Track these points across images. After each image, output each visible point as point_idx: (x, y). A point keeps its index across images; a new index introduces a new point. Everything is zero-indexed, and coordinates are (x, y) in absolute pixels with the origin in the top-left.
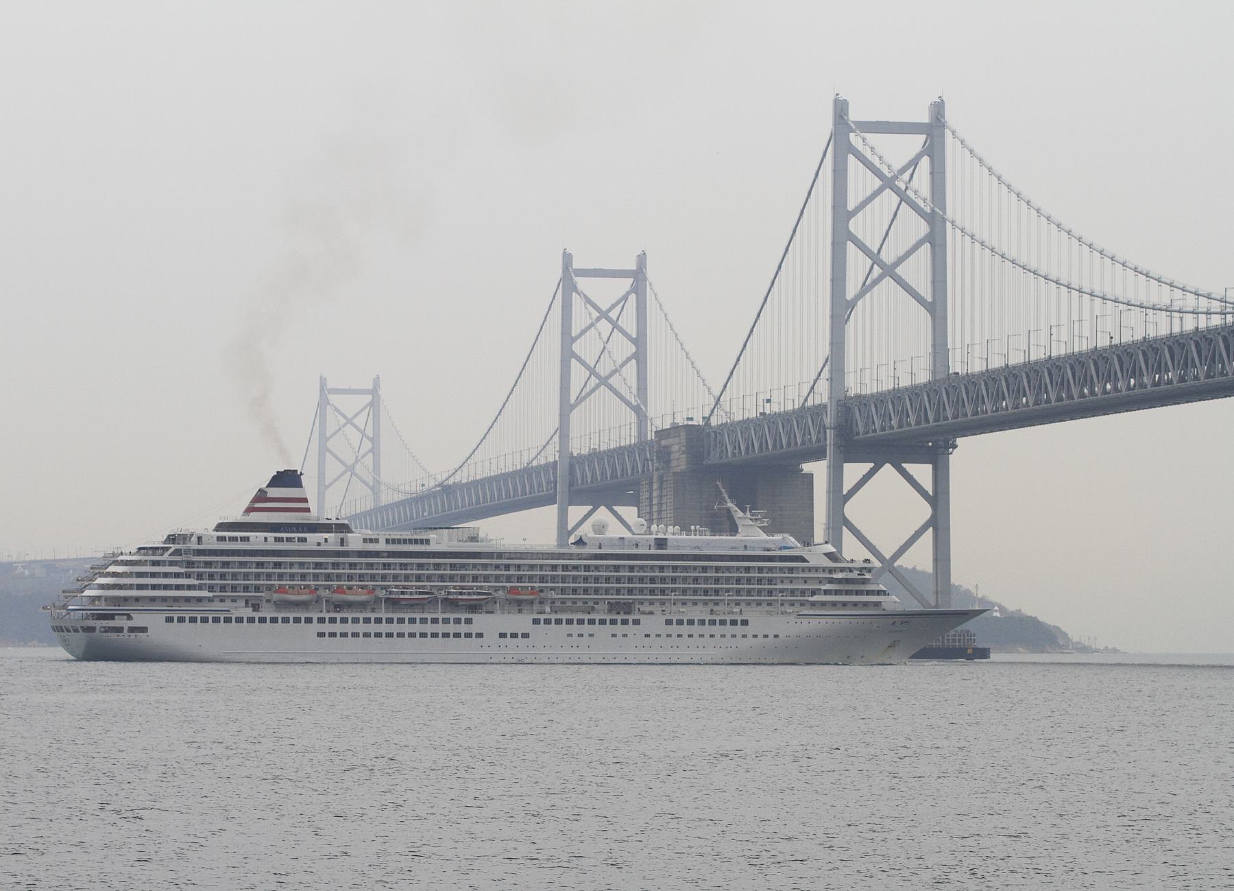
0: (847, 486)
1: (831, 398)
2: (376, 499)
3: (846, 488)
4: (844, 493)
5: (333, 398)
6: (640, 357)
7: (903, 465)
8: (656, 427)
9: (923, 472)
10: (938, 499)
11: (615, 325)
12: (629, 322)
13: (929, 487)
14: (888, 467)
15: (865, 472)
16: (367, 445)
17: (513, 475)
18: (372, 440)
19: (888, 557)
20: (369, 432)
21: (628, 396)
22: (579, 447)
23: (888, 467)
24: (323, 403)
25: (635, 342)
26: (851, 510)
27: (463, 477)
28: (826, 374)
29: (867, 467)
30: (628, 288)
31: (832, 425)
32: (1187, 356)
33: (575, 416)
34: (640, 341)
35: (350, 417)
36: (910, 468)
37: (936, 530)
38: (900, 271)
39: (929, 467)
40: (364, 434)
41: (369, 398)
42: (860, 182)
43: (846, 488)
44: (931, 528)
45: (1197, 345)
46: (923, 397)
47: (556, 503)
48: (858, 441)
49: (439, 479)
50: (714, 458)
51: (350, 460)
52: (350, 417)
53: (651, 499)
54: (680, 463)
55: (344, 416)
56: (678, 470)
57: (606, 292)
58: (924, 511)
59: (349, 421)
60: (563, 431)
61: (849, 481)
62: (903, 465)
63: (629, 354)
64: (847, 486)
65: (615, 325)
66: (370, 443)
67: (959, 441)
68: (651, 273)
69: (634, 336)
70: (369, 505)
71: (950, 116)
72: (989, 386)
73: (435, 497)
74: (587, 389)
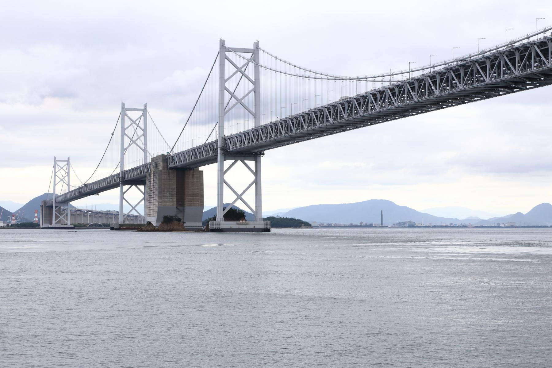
0: (225, 168)
1: (219, 137)
2: (69, 188)
3: (225, 169)
4: (224, 171)
5: (58, 163)
6: (145, 135)
7: (245, 161)
8: (152, 156)
9: (251, 163)
10: (257, 173)
11: (138, 126)
12: (142, 125)
13: (253, 169)
14: (239, 162)
15: (231, 163)
16: (67, 174)
17: (107, 178)
18: (67, 173)
19: (134, 207)
20: (67, 171)
21: (66, 183)
22: (126, 168)
23: (239, 162)
24: (55, 164)
25: (143, 130)
26: (125, 196)
27: (90, 182)
28: (120, 165)
29: (128, 186)
30: (141, 115)
31: (220, 146)
32: (234, 141)
33: (56, 186)
34: (145, 130)
35: (134, 120)
36: (247, 162)
37: (256, 184)
38: (60, 180)
39: (143, 186)
40: (66, 172)
41: (66, 163)
42: (229, 69)
43: (225, 169)
44: (255, 183)
45: (245, 135)
46: (243, 136)
47: (216, 161)
48: (229, 152)
49: (84, 183)
50: (172, 165)
51: (62, 178)
52: (134, 120)
53: (150, 182)
54: (161, 167)
55: (61, 167)
56: (159, 169)
57: (135, 115)
58: (252, 178)
59: (62, 168)
60: (122, 163)
61: (124, 190)
62: (245, 161)
63: (142, 134)
64: (225, 168)
65: (138, 126)
66: (143, 132)
67: (266, 152)
68: (70, 161)
69: (143, 128)
70: (67, 191)
71: (260, 46)
72: (178, 157)
73: (83, 188)
74: (292, 70)
